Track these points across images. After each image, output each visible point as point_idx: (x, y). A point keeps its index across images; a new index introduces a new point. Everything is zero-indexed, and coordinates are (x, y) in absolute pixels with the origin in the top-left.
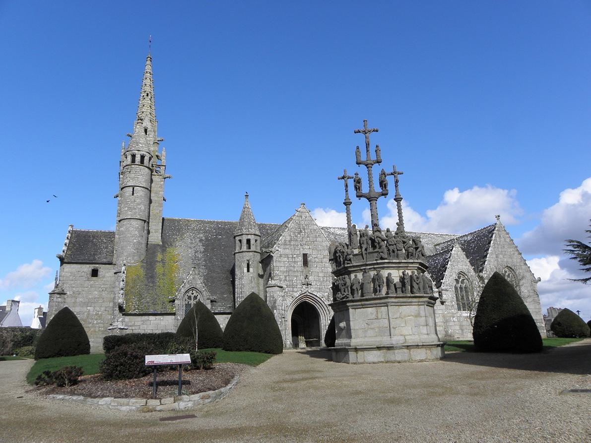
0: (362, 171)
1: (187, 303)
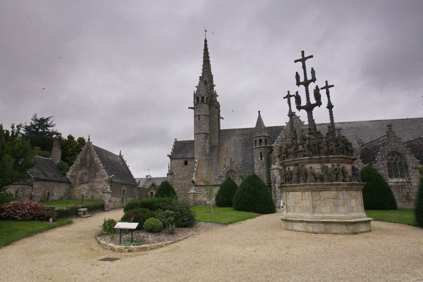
0: (301, 90)
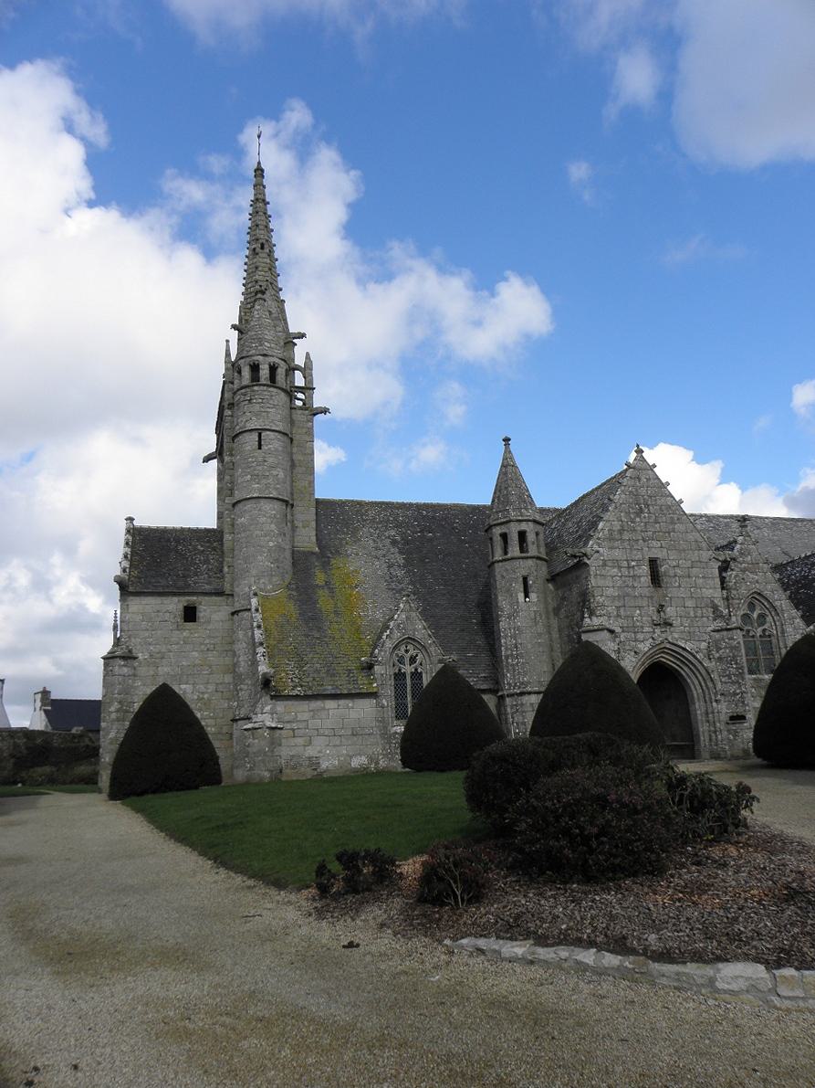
1: (397, 671)
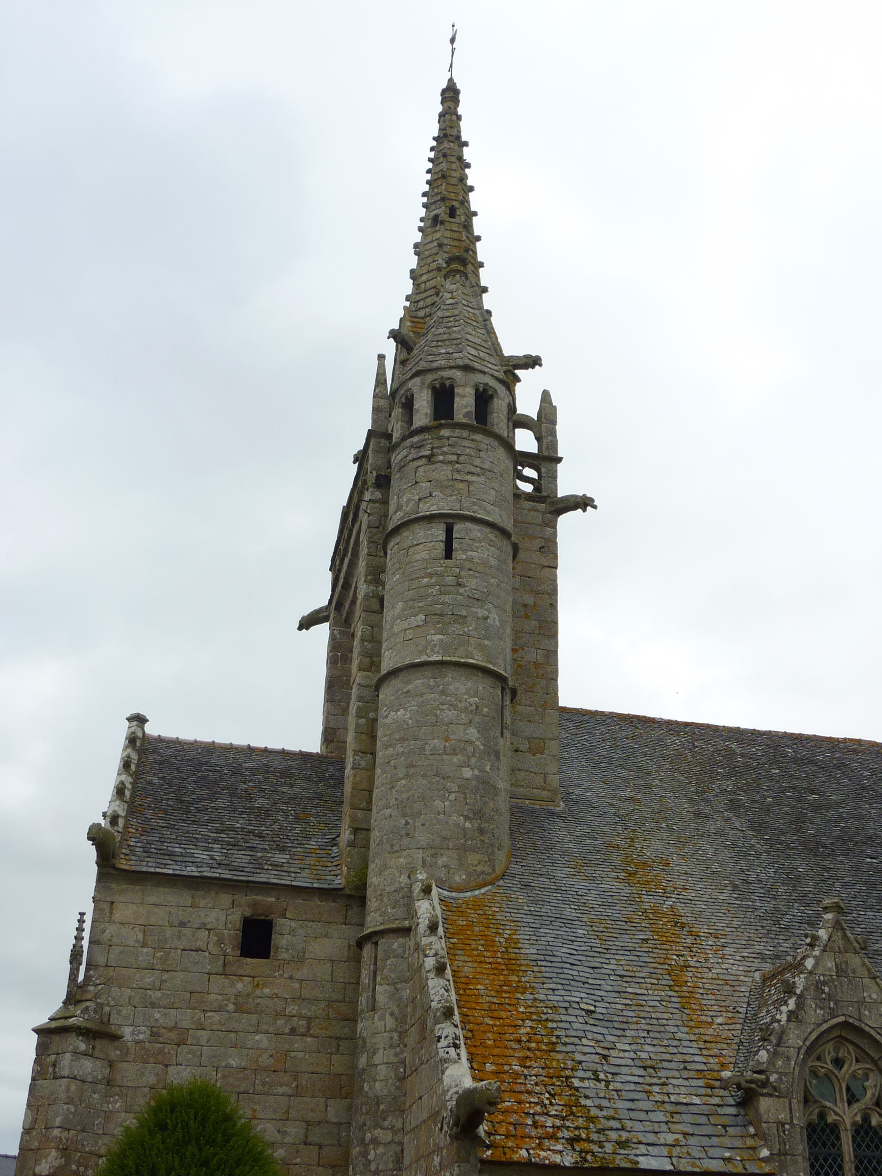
1: (815, 1117)
